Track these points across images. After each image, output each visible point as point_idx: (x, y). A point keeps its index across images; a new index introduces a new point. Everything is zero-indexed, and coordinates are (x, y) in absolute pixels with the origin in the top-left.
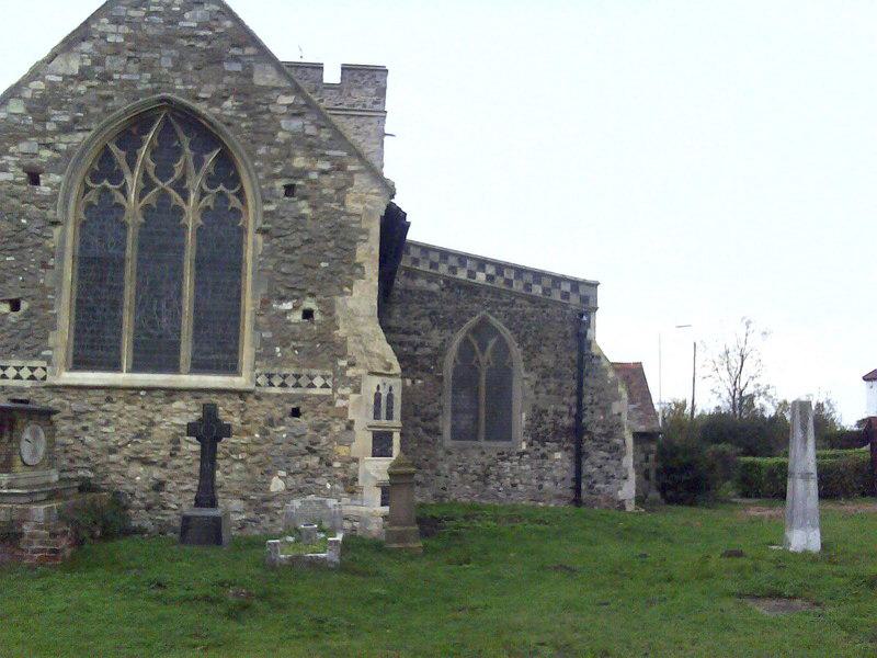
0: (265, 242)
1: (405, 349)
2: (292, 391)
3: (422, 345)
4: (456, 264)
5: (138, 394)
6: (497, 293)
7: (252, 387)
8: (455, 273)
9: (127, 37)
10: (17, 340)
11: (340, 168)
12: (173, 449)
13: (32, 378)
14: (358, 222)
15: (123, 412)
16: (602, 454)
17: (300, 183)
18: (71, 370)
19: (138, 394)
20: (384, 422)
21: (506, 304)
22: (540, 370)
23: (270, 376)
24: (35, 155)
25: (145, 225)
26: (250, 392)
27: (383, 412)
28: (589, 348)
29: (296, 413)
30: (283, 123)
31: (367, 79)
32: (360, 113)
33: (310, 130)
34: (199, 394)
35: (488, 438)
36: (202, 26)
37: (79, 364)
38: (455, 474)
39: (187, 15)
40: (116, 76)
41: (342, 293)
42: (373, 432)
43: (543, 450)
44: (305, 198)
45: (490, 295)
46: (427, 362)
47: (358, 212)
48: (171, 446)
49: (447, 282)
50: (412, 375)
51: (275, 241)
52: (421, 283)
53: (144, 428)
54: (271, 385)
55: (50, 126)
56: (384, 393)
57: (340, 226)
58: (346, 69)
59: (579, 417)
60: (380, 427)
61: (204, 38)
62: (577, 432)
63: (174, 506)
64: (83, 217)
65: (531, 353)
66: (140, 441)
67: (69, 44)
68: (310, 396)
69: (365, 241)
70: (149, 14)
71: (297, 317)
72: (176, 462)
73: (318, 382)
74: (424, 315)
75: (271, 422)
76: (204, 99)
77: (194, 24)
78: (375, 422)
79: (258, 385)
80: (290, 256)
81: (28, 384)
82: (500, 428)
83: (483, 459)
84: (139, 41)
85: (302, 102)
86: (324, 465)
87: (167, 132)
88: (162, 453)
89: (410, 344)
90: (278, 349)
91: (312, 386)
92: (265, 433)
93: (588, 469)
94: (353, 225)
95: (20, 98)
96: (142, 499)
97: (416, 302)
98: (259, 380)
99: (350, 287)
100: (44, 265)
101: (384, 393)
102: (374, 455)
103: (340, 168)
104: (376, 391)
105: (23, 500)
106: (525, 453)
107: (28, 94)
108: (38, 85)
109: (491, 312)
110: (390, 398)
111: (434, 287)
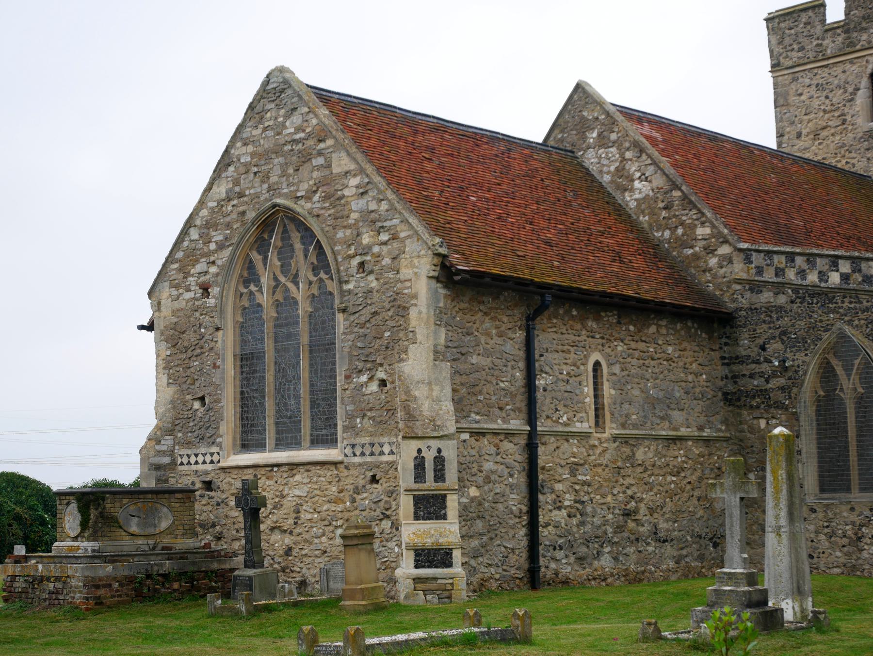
0: (345, 320)
1: (756, 383)
2: (369, 459)
4: (805, 266)
5: (272, 470)
6: (855, 294)
7: (340, 458)
8: (804, 278)
9: (253, 155)
10: (202, 431)
11: (394, 237)
12: (296, 518)
13: (212, 462)
14: (410, 287)
15: (265, 487)
17: (368, 258)
18: (238, 453)
19: (272, 470)
20: (430, 484)
23: (353, 446)
24: (206, 273)
25: (278, 319)
26: (341, 463)
27: (430, 474)
29: (374, 480)
30: (354, 207)
32: (797, 69)
33: (373, 206)
34: (308, 467)
35: (863, 489)
36: (299, 129)
37: (245, 447)
38: (822, 537)
39: (288, 124)
40: (247, 193)
41: (401, 360)
42: (414, 495)
45: (846, 300)
46: (781, 396)
47: (408, 277)
48: (295, 515)
49: (796, 289)
50: (765, 416)
51: (352, 318)
52: (767, 296)
54: (355, 455)
55: (213, 246)
56: (429, 456)
57: (397, 294)
60: (422, 490)
61: (295, 141)
63: (298, 570)
64: (310, 310)
66: (275, 511)
67: (214, 172)
69: (416, 305)
70: (265, 129)
71: (374, 387)
72: (298, 530)
73: (386, 449)
74: (774, 338)
75: (357, 491)
76: (302, 197)
77: (292, 130)
78: (417, 486)
79: (346, 456)
80: (363, 330)
81: (209, 467)
83: (853, 517)
84: (260, 156)
85: (367, 180)
86: (394, 530)
89: (761, 375)
90: (358, 420)
91: (382, 453)
92: (353, 501)
94: (406, 291)
95: (195, 226)
96: (279, 563)
97: (764, 321)
98: (346, 451)
99: (406, 352)
100: (215, 366)
101: (429, 456)
102: (417, 517)
103: (394, 237)
104: (416, 454)
105: (160, 558)
107: (198, 222)
108: (204, 212)
109: (850, 323)
110: (439, 461)
111: (782, 300)
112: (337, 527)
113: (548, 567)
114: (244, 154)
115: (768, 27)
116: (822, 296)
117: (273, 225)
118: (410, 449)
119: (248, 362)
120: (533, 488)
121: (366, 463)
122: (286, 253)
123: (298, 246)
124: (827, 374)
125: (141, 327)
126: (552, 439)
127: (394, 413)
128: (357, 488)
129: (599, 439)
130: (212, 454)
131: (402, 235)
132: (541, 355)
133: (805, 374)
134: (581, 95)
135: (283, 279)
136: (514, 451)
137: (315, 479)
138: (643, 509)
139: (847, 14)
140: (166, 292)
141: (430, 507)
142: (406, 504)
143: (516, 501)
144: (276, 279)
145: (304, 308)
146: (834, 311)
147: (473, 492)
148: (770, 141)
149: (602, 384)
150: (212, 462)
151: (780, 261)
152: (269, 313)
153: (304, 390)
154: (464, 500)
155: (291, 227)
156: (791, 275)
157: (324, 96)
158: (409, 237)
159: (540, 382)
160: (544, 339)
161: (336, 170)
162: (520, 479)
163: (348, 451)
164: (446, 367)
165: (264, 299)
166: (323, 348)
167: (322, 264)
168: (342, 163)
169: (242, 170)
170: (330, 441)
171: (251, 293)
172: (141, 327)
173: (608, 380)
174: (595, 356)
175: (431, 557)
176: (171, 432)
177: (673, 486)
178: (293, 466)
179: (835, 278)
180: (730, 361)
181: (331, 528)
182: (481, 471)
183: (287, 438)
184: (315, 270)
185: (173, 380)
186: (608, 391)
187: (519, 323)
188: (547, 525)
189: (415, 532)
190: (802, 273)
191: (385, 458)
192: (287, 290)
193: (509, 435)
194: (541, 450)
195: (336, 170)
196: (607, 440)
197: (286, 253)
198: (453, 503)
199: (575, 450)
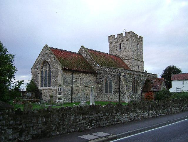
35: (109, 93)
37: (41, 87)
58: (126, 33)
59: (119, 89)
62: (119, 91)
65: (114, 80)
71: (55, 81)
82: (111, 92)
110: (61, 89)
113: (73, 101)
114: (42, 54)
116: (106, 71)
117: (45, 62)
118: (58, 87)
119: (42, 77)
120: (72, 92)
122: (46, 66)
123: (47, 65)
124: (106, 80)
127: (56, 84)
134: (82, 47)
136: (70, 88)
140: (33, 69)
141: (60, 94)
142: (57, 93)
143: (70, 93)
145: (48, 72)
148: (107, 51)
151: (104, 68)
153: (47, 81)
155: (47, 63)
156: (103, 69)
157: (51, 48)
160: (74, 76)
162: (70, 91)
164: (62, 79)
165: (44, 70)
166: (50, 76)
167: (50, 67)
168: (52, 56)
174: (80, 78)
175: (60, 99)
178: (46, 89)
179: (107, 70)
180: (96, 78)
183: (46, 86)
184: (49, 68)
189: (58, 96)
190: (104, 69)
197: (46, 66)
198: (62, 93)
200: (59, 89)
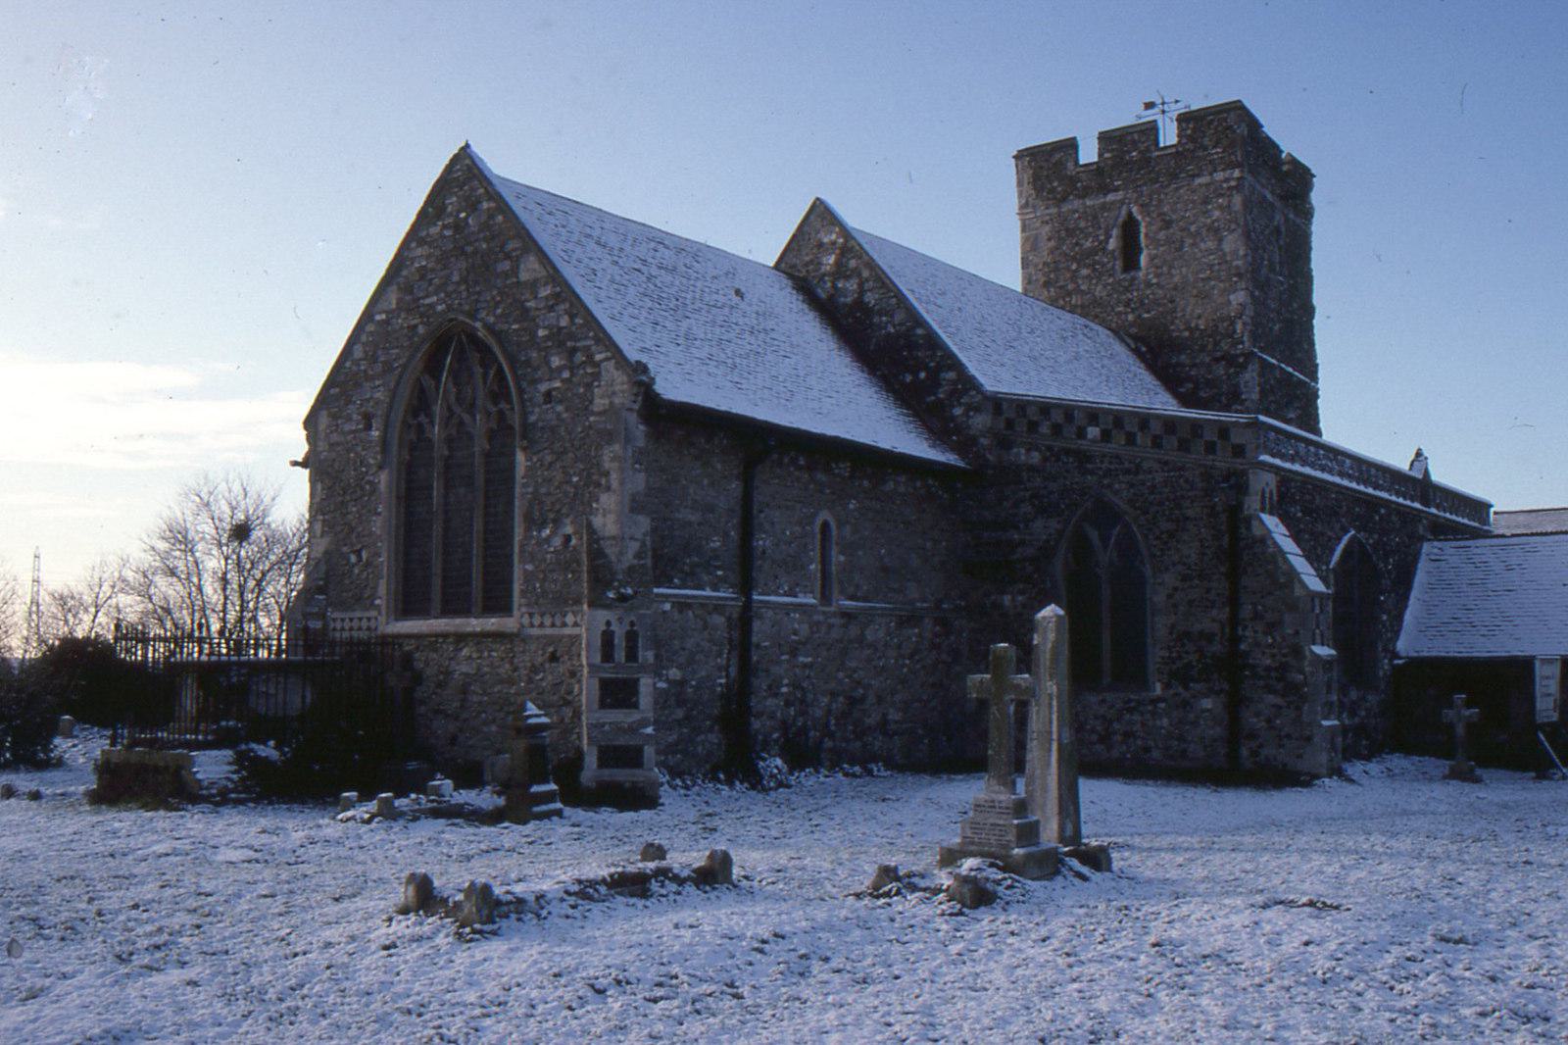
2: (549, 631)
3: (1022, 543)
16: (1272, 699)
18: (397, 620)
21: (1128, 472)
22: (1180, 568)
27: (620, 655)
28: (1249, 528)
29: (554, 658)
31: (1074, 139)
43: (1186, 695)
44: (560, 402)
53: (441, 677)
56: (619, 632)
58: (1184, 119)
64: (446, 453)
66: (439, 691)
68: (563, 636)
87: (461, 357)
88: (454, 705)
91: (564, 625)
93: (1251, 720)
106: (1160, 699)
108: (371, 328)
112: (508, 713)
115: (1017, 166)
121: (545, 636)
125: (295, 464)
126: (770, 613)
128: (533, 665)
129: (824, 613)
130: (369, 619)
131: (598, 357)
132: (761, 512)
133: (580, 694)
135: (458, 410)
137: (486, 654)
138: (871, 699)
139: (1100, 155)
144: (449, 408)
146: (1092, 473)
147: (674, 673)
149: (830, 549)
150: (369, 629)
152: (440, 450)
154: (662, 685)
158: (607, 359)
159: (761, 542)
161: (524, 276)
163: (526, 620)
169: (1181, 984)
170: (503, 607)
171: (420, 425)
172: (295, 464)
173: (837, 544)
174: (825, 515)
176: (321, 590)
177: (905, 670)
178: (461, 638)
181: (502, 715)
182: (684, 649)
185: (329, 527)
186: (837, 558)
187: (735, 472)
188: (759, 715)
191: (567, 631)
192: (461, 423)
193: (718, 608)
194: (756, 625)
195: (524, 276)
196: (834, 615)
198: (646, 684)
199: (796, 626)
200: (608, 639)
